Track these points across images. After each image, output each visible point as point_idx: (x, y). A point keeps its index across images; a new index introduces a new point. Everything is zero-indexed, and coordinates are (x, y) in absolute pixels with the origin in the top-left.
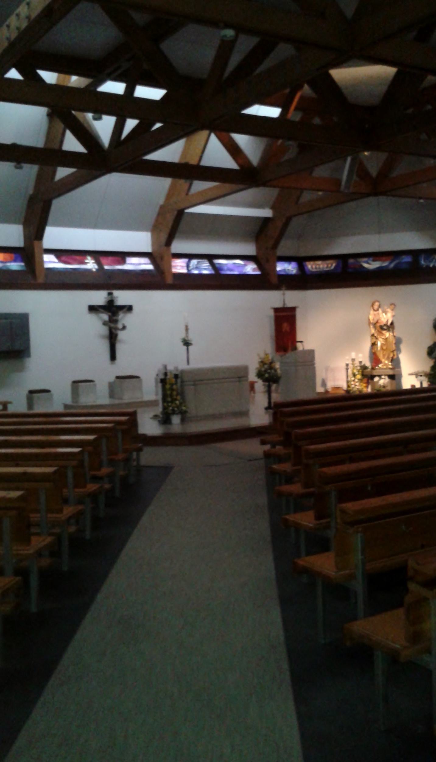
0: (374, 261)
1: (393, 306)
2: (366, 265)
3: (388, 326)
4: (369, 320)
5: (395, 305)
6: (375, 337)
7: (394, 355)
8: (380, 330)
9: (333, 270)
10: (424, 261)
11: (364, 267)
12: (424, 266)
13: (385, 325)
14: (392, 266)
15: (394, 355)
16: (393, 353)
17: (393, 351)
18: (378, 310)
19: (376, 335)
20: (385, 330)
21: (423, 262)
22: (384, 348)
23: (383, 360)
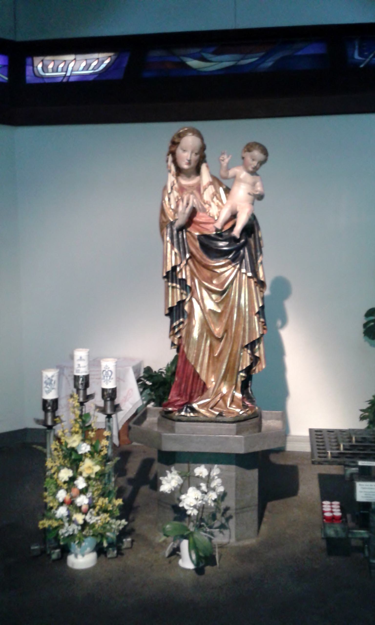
0: (217, 53)
1: (257, 154)
2: (193, 63)
3: (233, 240)
4: (163, 212)
5: (265, 151)
6: (183, 282)
7: (255, 360)
8: (200, 254)
9: (101, 73)
10: (360, 54)
11: (189, 68)
12: (124, 540)
13: (220, 235)
14: (269, 63)
15: (255, 360)
16: (253, 353)
17: (252, 345)
18: (197, 171)
19: (184, 275)
20: (223, 254)
21: (357, 56)
22: (218, 330)
23: (212, 382)
